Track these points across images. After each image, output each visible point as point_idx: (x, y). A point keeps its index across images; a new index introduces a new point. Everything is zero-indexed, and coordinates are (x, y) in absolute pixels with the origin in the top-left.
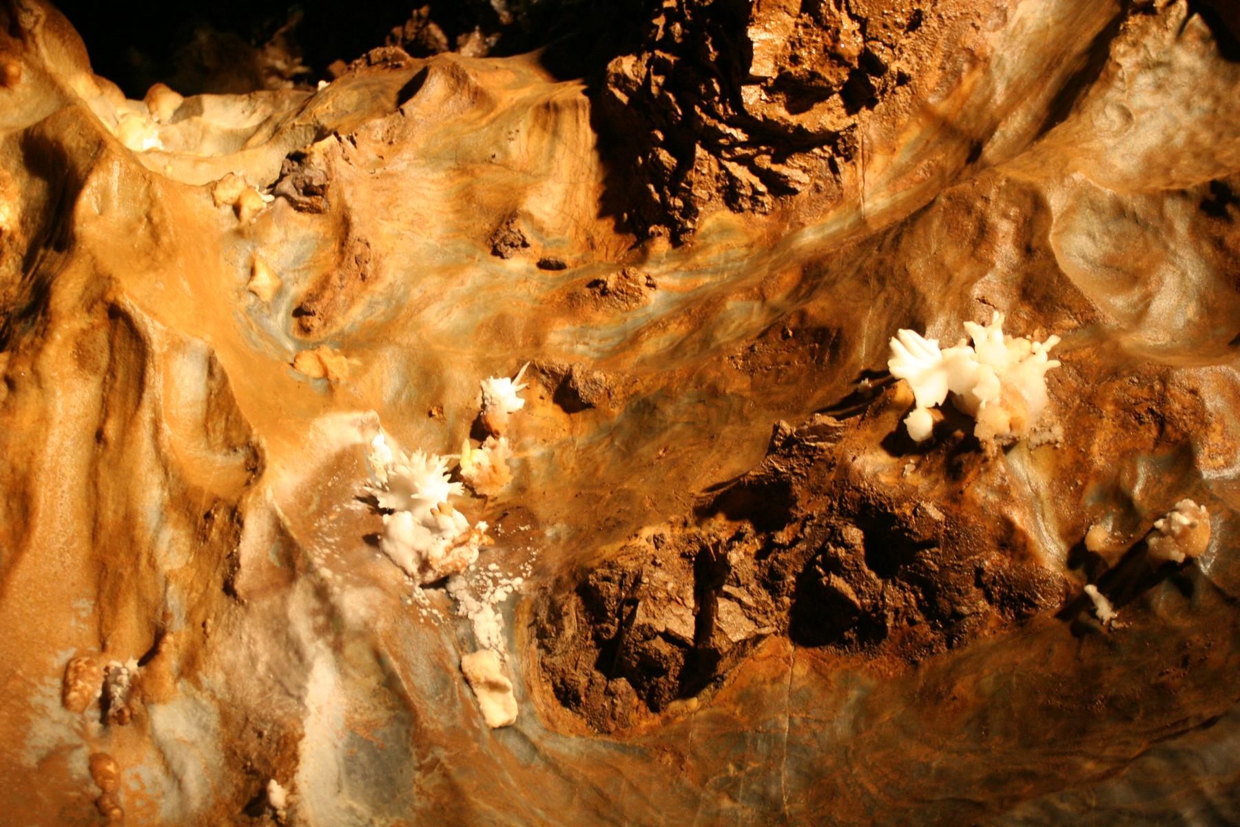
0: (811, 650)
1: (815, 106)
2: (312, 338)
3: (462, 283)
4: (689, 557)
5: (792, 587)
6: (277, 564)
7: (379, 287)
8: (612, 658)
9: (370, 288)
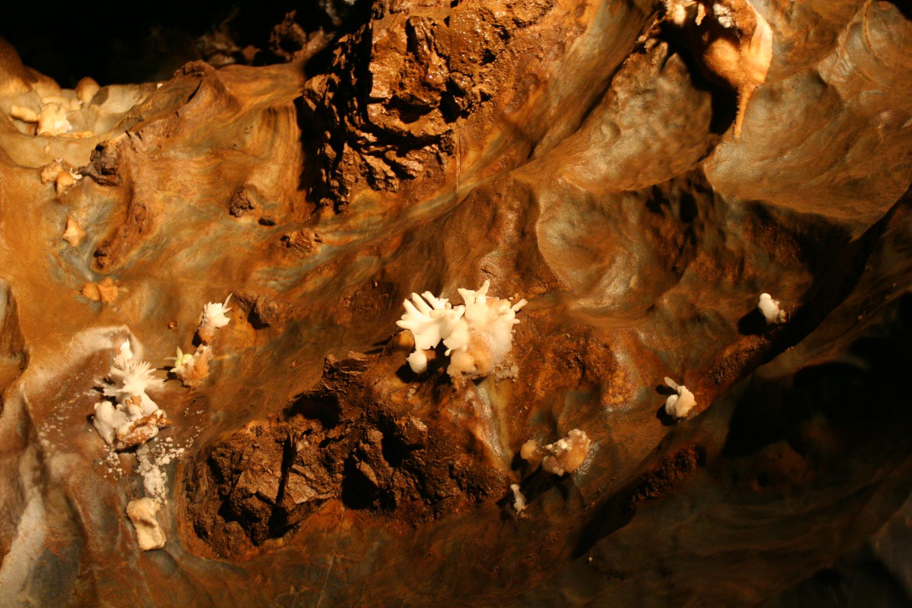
0: (355, 511)
1: (421, 117)
2: (104, 272)
3: (207, 234)
4: (281, 442)
5: (342, 468)
6: (20, 434)
7: (150, 237)
8: (227, 511)
9: (144, 237)
